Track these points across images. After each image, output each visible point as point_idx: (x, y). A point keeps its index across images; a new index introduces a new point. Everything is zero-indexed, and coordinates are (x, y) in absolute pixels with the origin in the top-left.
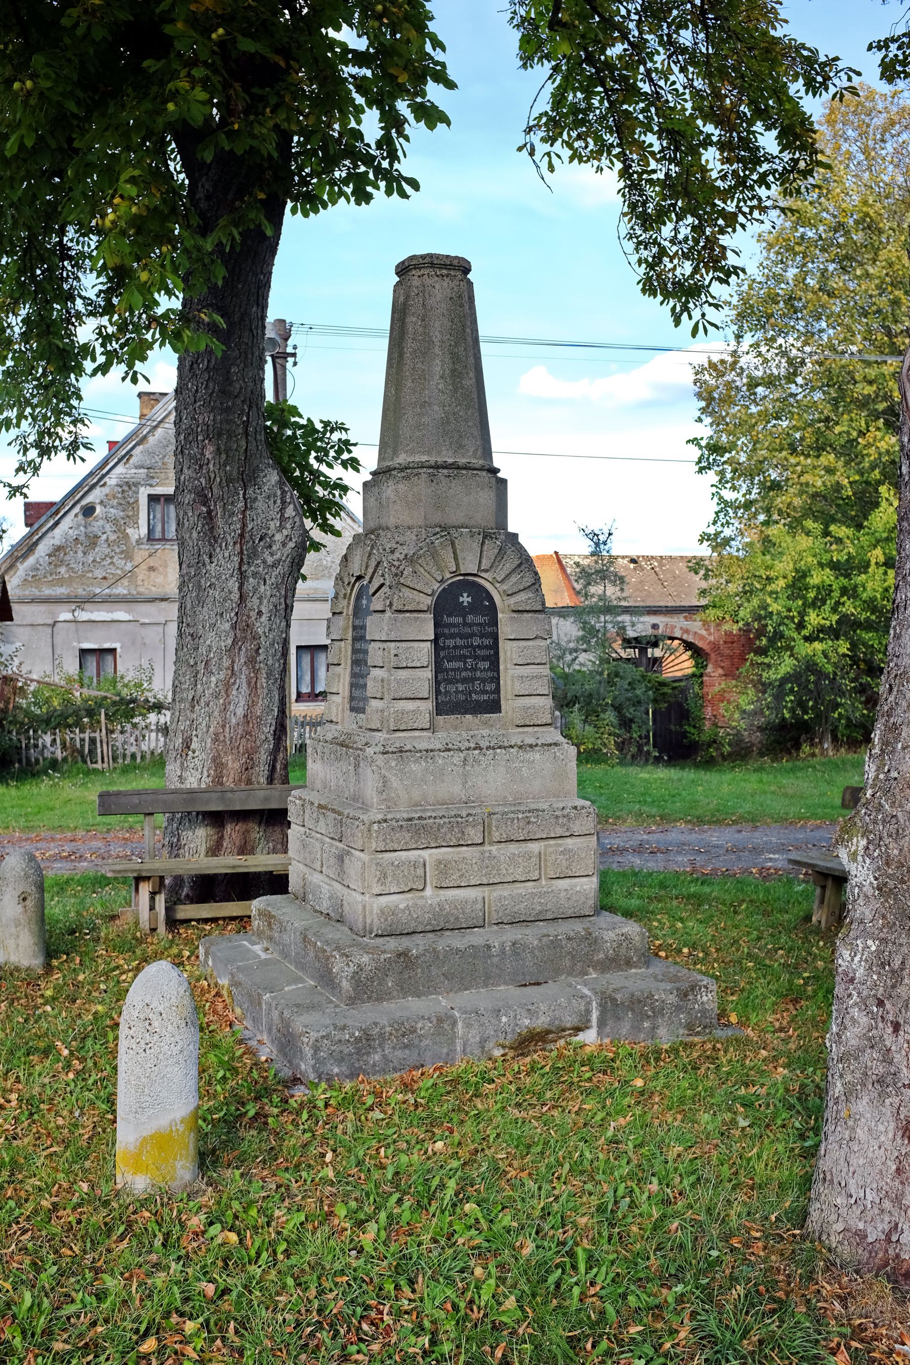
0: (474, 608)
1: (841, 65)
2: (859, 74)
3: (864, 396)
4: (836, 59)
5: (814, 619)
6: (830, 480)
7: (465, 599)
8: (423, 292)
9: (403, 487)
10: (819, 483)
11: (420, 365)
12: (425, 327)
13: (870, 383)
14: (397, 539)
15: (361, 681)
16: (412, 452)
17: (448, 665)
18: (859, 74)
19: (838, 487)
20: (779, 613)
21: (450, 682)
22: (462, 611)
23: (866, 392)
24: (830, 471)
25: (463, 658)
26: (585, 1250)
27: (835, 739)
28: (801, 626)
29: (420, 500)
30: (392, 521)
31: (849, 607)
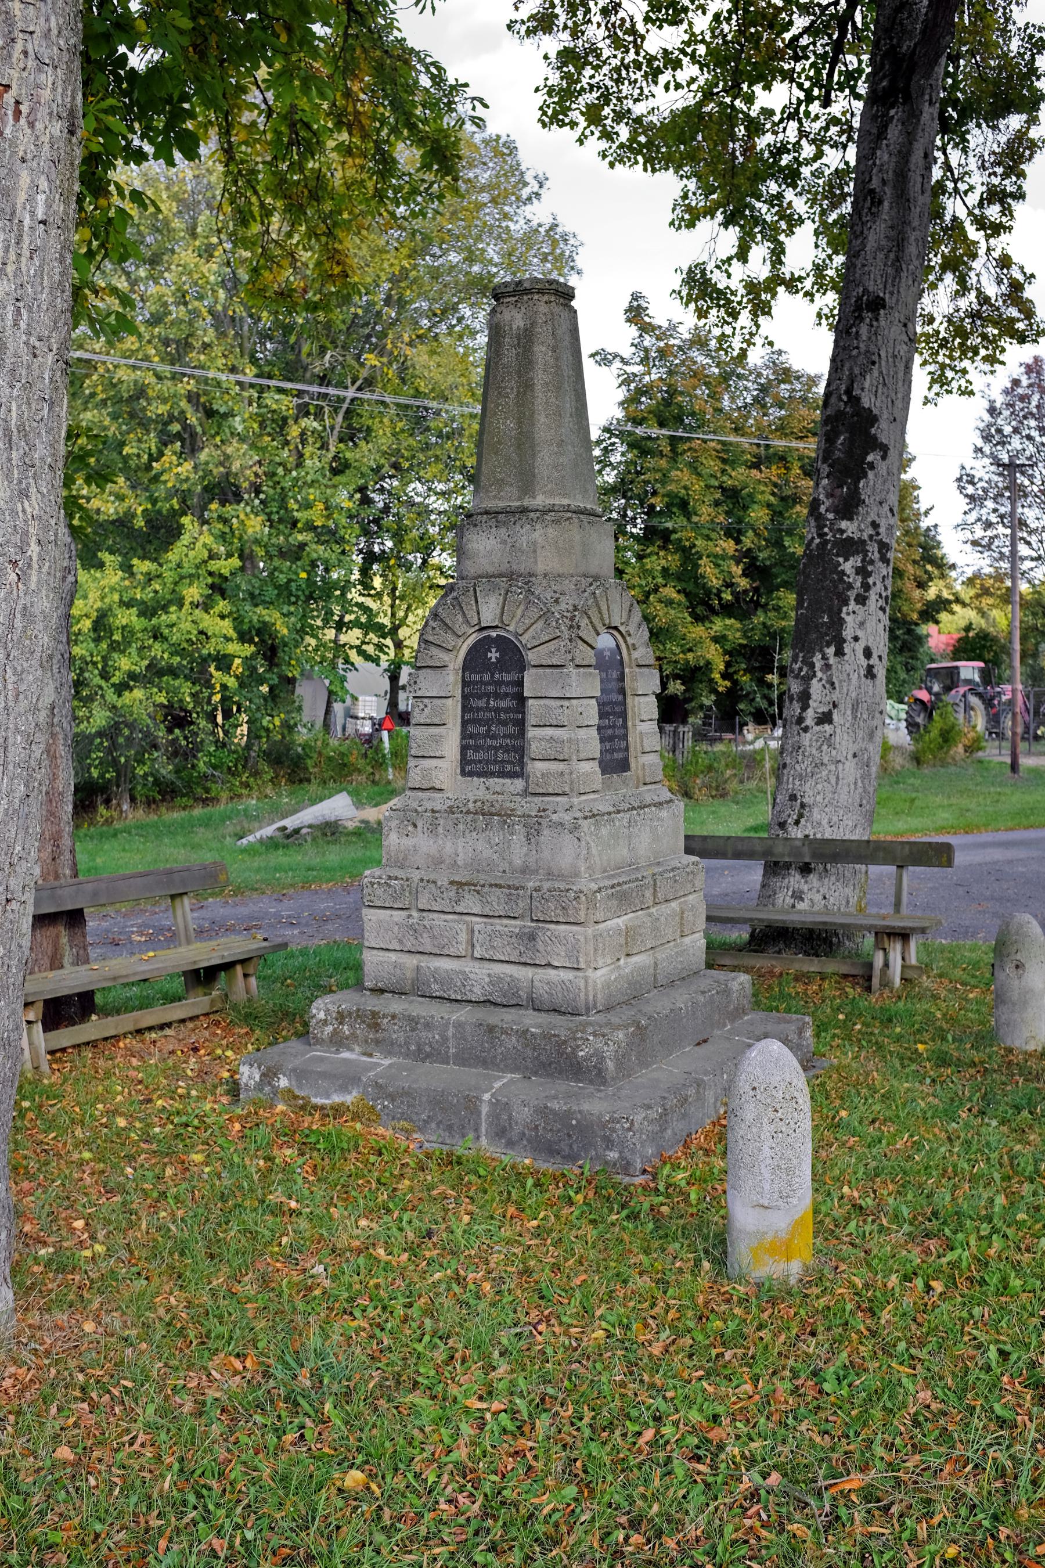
0: (501, 665)
1: (470, 92)
2: (486, 106)
3: (158, 416)
4: (466, 85)
5: (125, 663)
6: (122, 507)
7: (494, 655)
8: (552, 320)
9: (551, 531)
10: (112, 511)
11: (553, 400)
12: (557, 359)
13: (165, 401)
14: (555, 588)
15: (608, 745)
16: (551, 494)
17: (511, 729)
18: (486, 106)
19: (130, 515)
20: (82, 658)
21: (477, 749)
22: (488, 667)
23: (160, 412)
24: (121, 498)
25: (488, 722)
26: (960, 1257)
27: (133, 799)
28: (105, 675)
29: (573, 547)
30: (540, 568)
31: (157, 650)
